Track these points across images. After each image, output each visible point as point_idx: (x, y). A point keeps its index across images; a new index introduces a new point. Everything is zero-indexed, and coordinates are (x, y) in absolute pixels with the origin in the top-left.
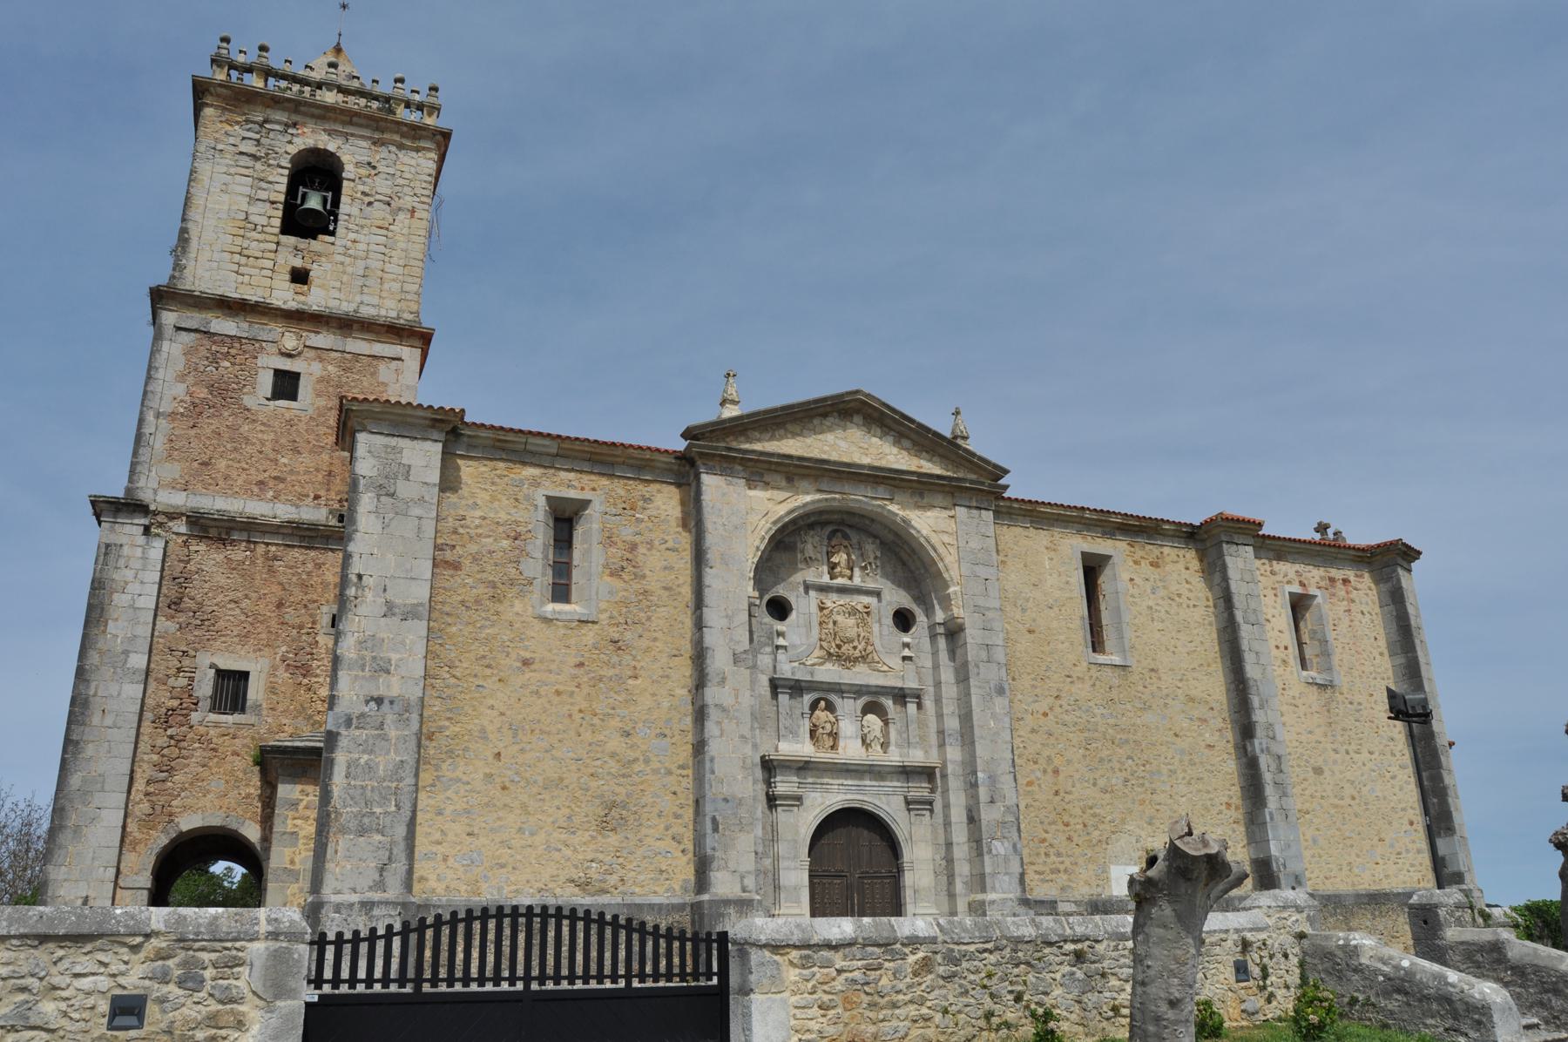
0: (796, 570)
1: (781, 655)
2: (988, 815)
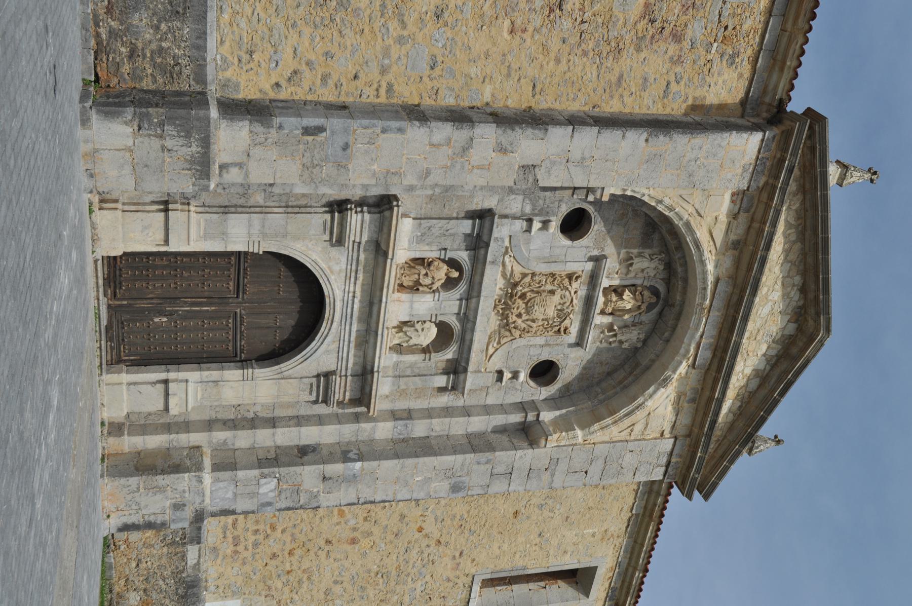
0: (618, 247)
1: (520, 225)
2: (308, 475)
